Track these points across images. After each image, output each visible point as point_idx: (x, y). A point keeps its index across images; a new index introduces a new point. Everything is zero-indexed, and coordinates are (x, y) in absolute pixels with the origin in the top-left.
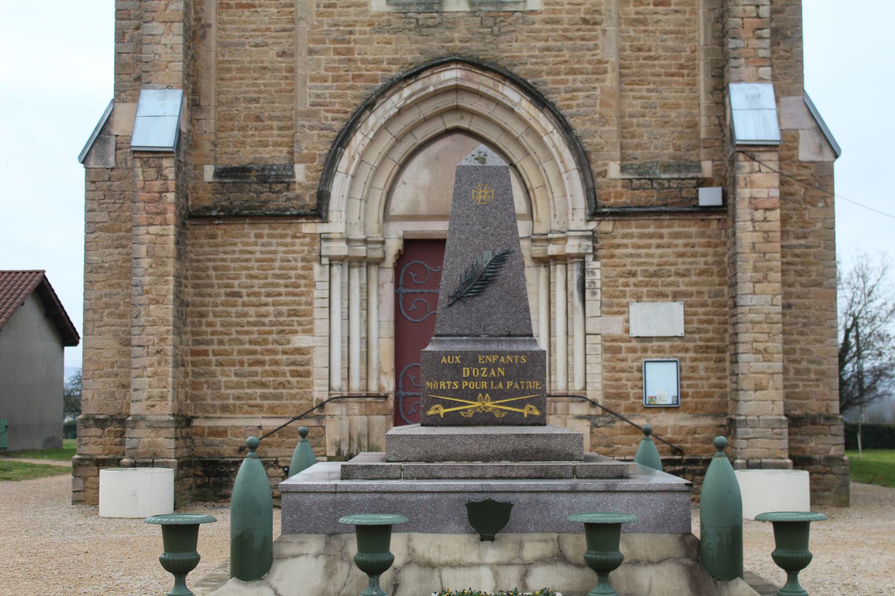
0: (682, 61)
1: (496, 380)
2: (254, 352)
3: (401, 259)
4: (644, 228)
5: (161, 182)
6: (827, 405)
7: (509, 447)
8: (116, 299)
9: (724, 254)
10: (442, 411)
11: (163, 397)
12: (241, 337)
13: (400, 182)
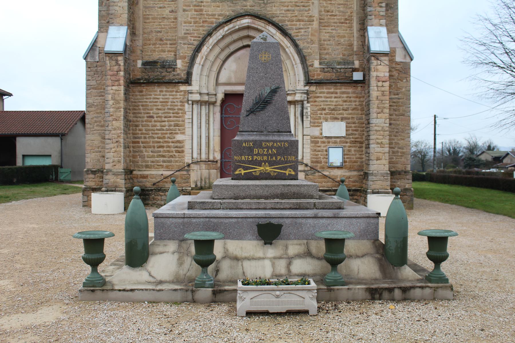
0: (347, 17)
1: (272, 156)
2: (159, 142)
3: (223, 102)
4: (329, 89)
5: (118, 67)
6: (405, 167)
7: (279, 192)
8: (100, 119)
9: (363, 101)
10: (243, 172)
11: (119, 162)
12: (154, 135)
13: (223, 69)
